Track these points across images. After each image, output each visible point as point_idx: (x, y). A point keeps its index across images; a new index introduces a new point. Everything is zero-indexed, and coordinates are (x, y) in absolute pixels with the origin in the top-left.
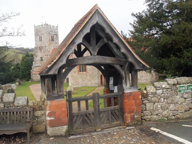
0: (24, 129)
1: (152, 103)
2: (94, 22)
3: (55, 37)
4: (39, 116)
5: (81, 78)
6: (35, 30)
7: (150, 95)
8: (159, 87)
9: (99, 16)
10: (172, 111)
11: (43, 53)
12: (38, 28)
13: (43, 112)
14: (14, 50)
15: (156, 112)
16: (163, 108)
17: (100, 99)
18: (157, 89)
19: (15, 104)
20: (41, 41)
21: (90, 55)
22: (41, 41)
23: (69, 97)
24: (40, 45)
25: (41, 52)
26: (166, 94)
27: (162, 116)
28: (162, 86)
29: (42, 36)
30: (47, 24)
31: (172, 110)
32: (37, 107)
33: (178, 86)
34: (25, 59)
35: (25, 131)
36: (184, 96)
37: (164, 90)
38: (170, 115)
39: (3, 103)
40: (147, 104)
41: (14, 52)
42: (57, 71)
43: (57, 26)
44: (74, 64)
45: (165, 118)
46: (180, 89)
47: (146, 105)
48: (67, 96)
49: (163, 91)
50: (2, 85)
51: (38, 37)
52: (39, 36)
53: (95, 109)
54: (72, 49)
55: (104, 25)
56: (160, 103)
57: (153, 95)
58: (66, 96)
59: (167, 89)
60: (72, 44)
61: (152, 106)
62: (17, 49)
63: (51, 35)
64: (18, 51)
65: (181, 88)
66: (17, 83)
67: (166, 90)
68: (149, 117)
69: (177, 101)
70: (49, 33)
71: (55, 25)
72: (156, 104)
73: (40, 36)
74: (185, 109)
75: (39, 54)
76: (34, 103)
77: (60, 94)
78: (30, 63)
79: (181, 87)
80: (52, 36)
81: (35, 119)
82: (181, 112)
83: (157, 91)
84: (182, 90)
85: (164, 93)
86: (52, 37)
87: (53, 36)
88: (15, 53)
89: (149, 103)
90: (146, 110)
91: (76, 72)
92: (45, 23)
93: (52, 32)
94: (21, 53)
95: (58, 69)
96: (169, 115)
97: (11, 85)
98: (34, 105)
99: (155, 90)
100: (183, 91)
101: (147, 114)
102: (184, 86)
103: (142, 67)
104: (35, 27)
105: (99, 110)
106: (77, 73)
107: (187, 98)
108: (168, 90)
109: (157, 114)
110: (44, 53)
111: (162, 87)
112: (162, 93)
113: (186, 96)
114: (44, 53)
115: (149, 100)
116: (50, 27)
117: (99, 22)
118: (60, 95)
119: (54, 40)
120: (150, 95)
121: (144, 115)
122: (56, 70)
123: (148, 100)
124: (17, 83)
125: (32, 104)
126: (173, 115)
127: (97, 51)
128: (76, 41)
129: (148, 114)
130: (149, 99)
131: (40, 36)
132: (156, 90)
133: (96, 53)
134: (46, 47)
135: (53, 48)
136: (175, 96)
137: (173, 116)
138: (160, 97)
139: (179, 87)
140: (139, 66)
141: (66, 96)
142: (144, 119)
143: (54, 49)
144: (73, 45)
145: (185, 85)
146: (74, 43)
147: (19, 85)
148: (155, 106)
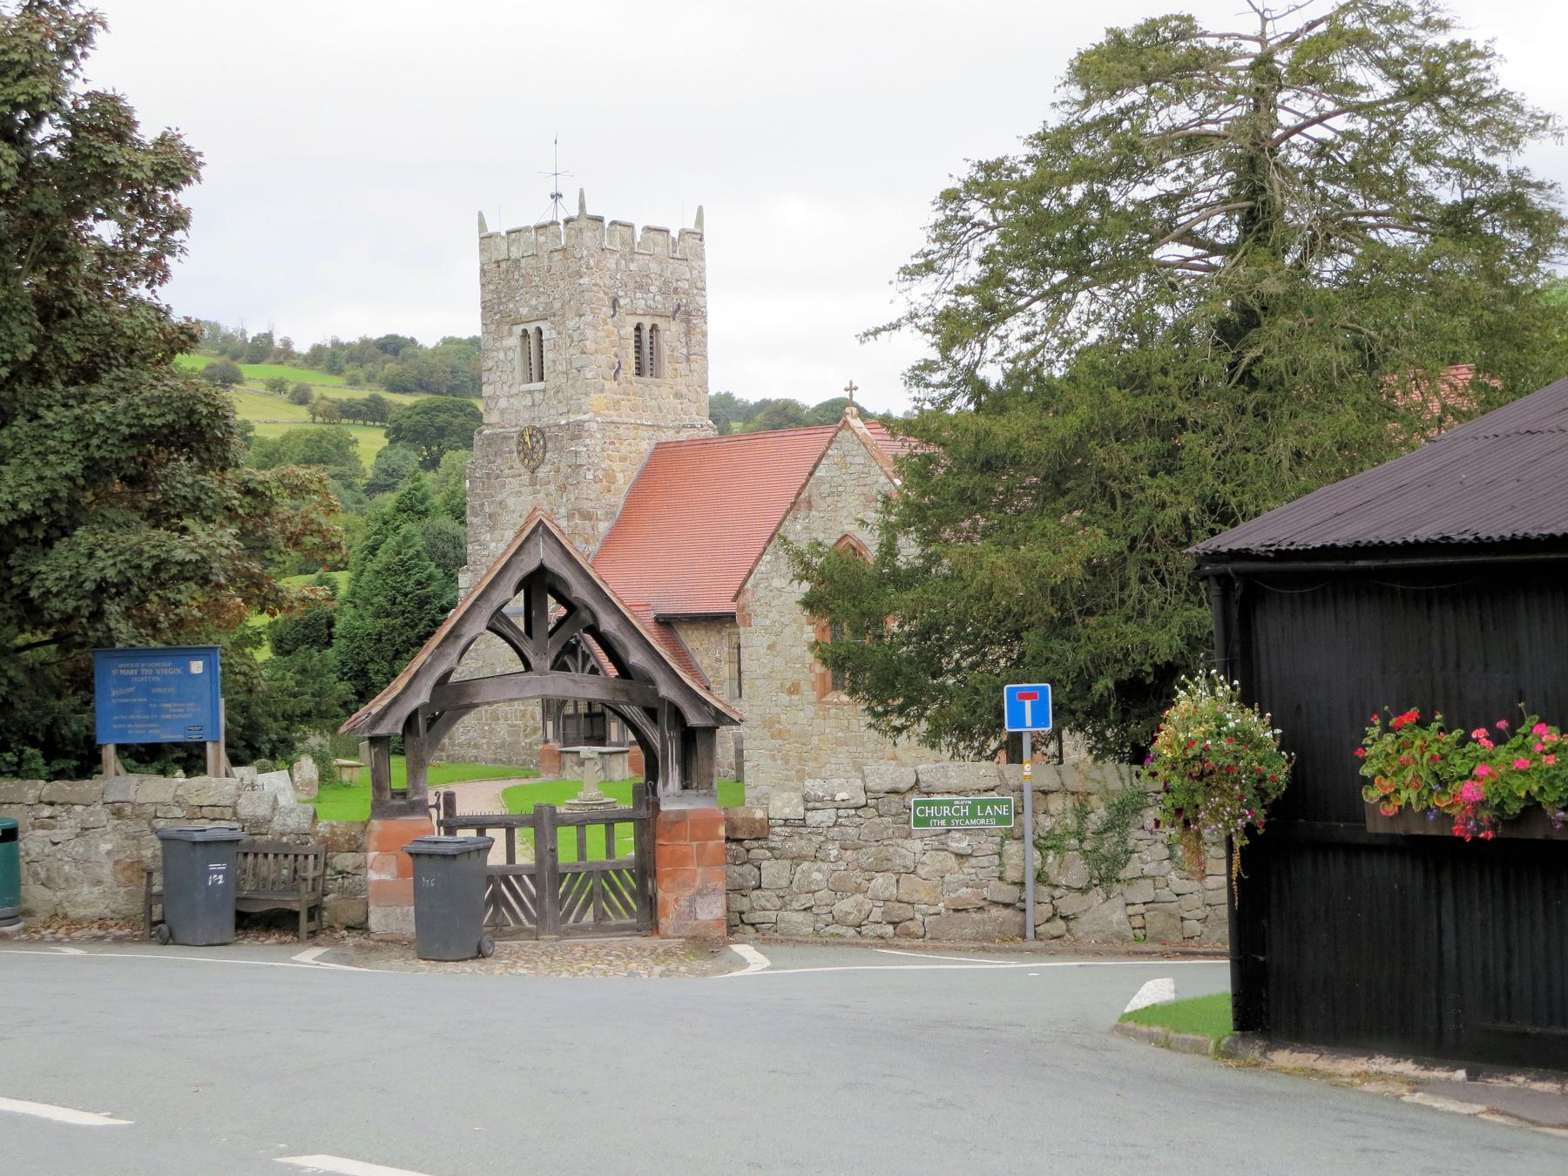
0: (297, 903)
1: (787, 863)
2: (528, 565)
3: (671, 332)
4: (349, 870)
5: (839, 743)
6: (483, 272)
7: (777, 829)
8: (821, 800)
9: (550, 542)
10: (881, 904)
11: (552, 488)
12: (515, 254)
13: (359, 857)
14: (294, 376)
15: (802, 897)
16: (838, 889)
17: (532, 830)
18: (810, 805)
19: (273, 825)
20: (541, 379)
21: (521, 668)
22: (541, 379)
23: (446, 814)
24: (525, 419)
25: (533, 483)
26: (852, 831)
27: (830, 919)
28: (833, 796)
29: (543, 326)
30: (600, 220)
31: (881, 896)
32: (342, 840)
33: (912, 799)
34: (392, 541)
35: (295, 906)
36: (954, 845)
37: (841, 812)
38: (871, 919)
39: (238, 820)
40: (765, 864)
41: (301, 398)
42: (401, 726)
43: (691, 226)
44: (466, 702)
45: (842, 930)
46: (922, 812)
47: (759, 869)
48: (438, 809)
49: (839, 817)
50: (849, 625)
51: (514, 341)
52: (518, 330)
53: (540, 859)
54: (449, 654)
55: (565, 571)
56: (825, 866)
57: (789, 830)
58: (438, 809)
59: (857, 808)
60: (452, 639)
61: (787, 874)
62: (330, 359)
63: (635, 320)
64: (334, 389)
65: (933, 811)
66: (307, 768)
67: (853, 812)
68: (772, 915)
69: (909, 863)
70: (615, 303)
71: (676, 223)
72: (805, 865)
73: (531, 328)
74: (952, 901)
75: (511, 502)
76: (332, 826)
77: (416, 798)
78: (430, 577)
79: (930, 804)
80: (638, 328)
81: (336, 880)
82: (931, 911)
83: (809, 814)
84: (935, 817)
85: (841, 825)
86: (646, 334)
87: (654, 328)
88: (302, 412)
89: (773, 861)
90: (759, 887)
91: (805, 687)
92: (575, 213)
93: (641, 287)
94: (372, 412)
95: (404, 720)
96: (863, 916)
97: (262, 778)
98: (333, 833)
99: (801, 810)
100: (943, 822)
101: (763, 902)
102: (950, 803)
103: (714, 718)
104: (486, 239)
105: (554, 866)
106: (812, 696)
107: (971, 855)
108: (860, 812)
109: (810, 908)
110: (563, 488)
111: (833, 800)
112: (835, 824)
113: (965, 844)
114: (563, 488)
115: (774, 848)
116: (628, 242)
117: (548, 564)
118: (415, 802)
119: (667, 368)
120: (777, 829)
121: (753, 909)
122: (397, 723)
123: (771, 849)
124: (307, 768)
125: (328, 830)
126: (889, 919)
127: (553, 655)
128: (464, 630)
129: (768, 905)
130: (773, 845)
131: (531, 328)
132: (807, 809)
133: (549, 664)
134: (574, 437)
135: (646, 447)
136: (900, 841)
137: (889, 923)
138: (822, 839)
139: (917, 804)
140: (700, 712)
141: (437, 806)
142: (753, 925)
143: (653, 455)
144: (454, 643)
145: (954, 797)
146: (458, 637)
147: (322, 778)
148: (797, 876)
